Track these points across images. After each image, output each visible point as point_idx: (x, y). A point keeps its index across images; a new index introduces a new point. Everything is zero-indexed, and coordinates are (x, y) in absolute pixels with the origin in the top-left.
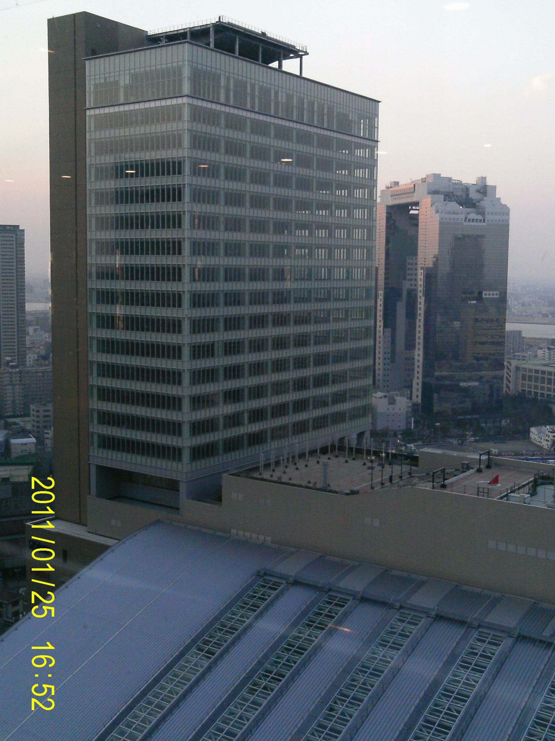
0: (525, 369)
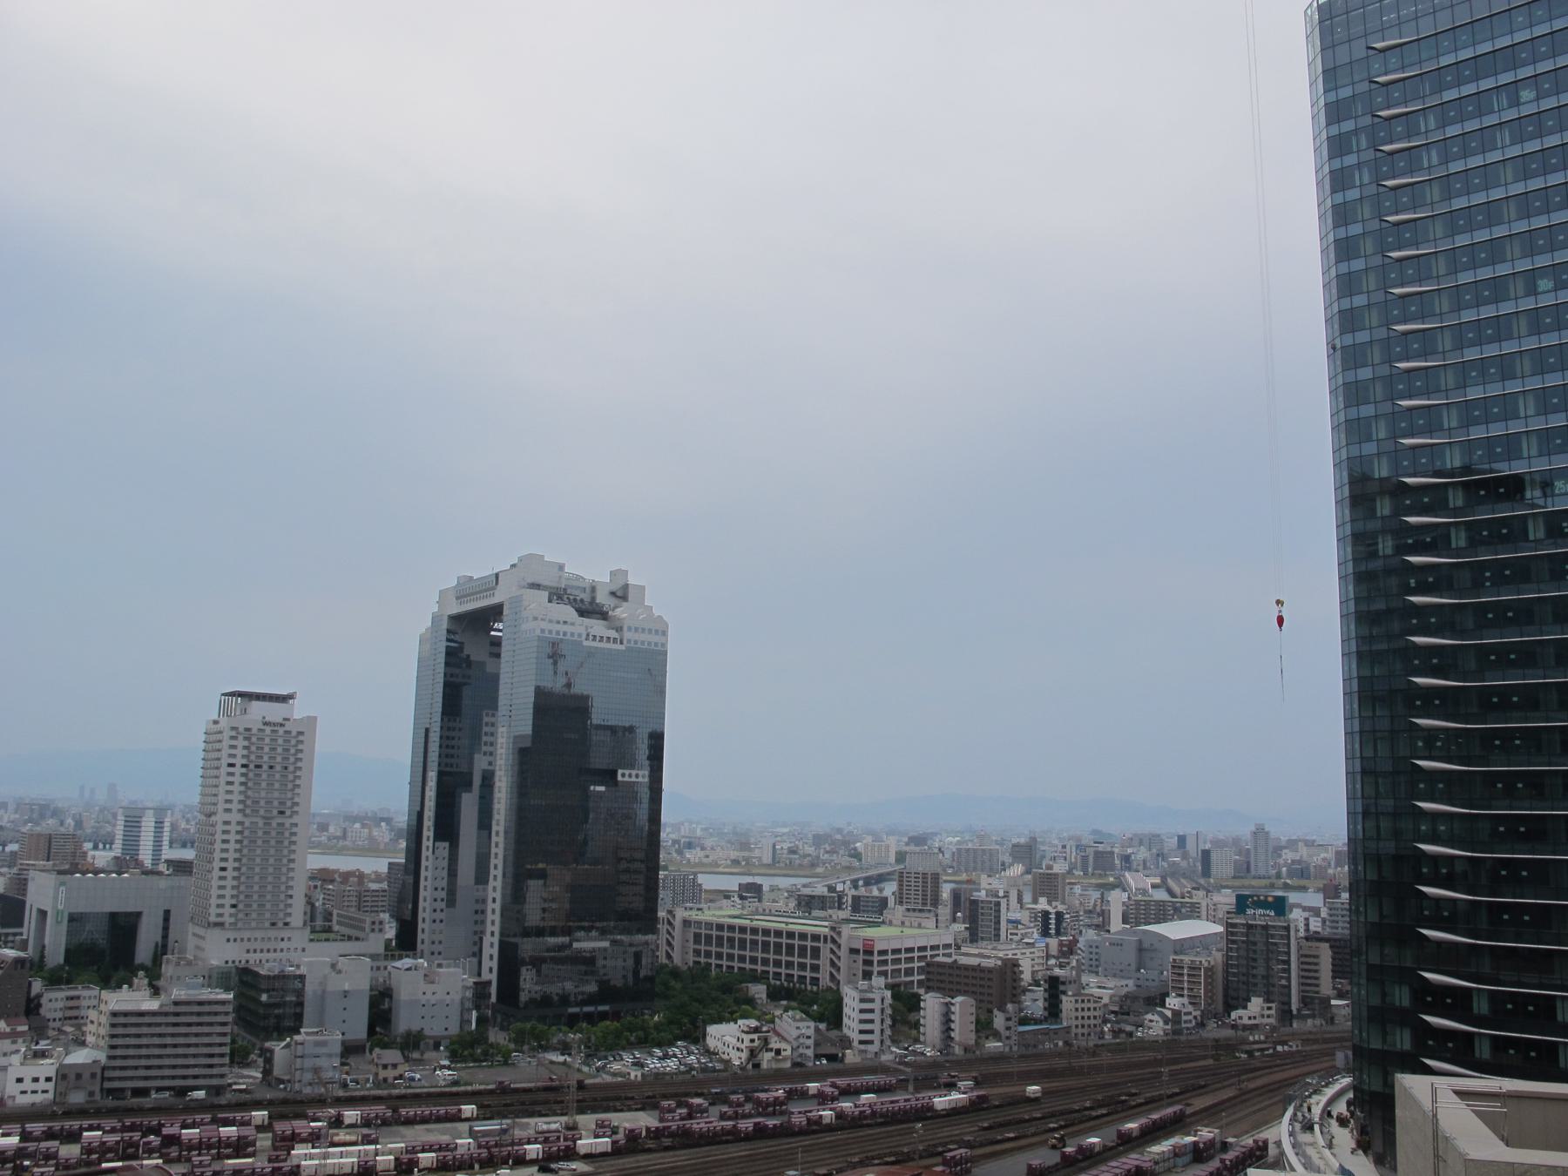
0: (699, 923)
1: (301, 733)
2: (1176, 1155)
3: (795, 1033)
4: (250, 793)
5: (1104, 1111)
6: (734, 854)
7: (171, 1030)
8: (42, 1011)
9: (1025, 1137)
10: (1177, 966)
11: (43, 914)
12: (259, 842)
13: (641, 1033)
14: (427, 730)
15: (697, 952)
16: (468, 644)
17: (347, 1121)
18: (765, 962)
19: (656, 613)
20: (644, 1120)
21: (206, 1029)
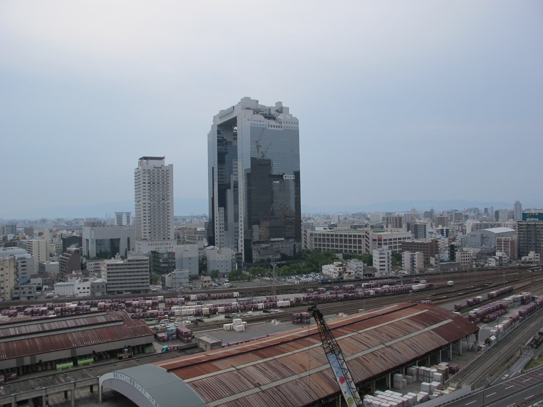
1: (168, 170)
2: (515, 302)
3: (356, 266)
4: (152, 193)
5: (480, 289)
6: (324, 221)
7: (128, 270)
8: (87, 268)
9: (450, 297)
10: (499, 241)
11: (87, 240)
12: (157, 210)
13: (298, 269)
14: (213, 168)
15: (316, 245)
16: (225, 132)
17: (192, 299)
18: (341, 246)
19: (294, 116)
20: (301, 296)
21: (140, 270)
